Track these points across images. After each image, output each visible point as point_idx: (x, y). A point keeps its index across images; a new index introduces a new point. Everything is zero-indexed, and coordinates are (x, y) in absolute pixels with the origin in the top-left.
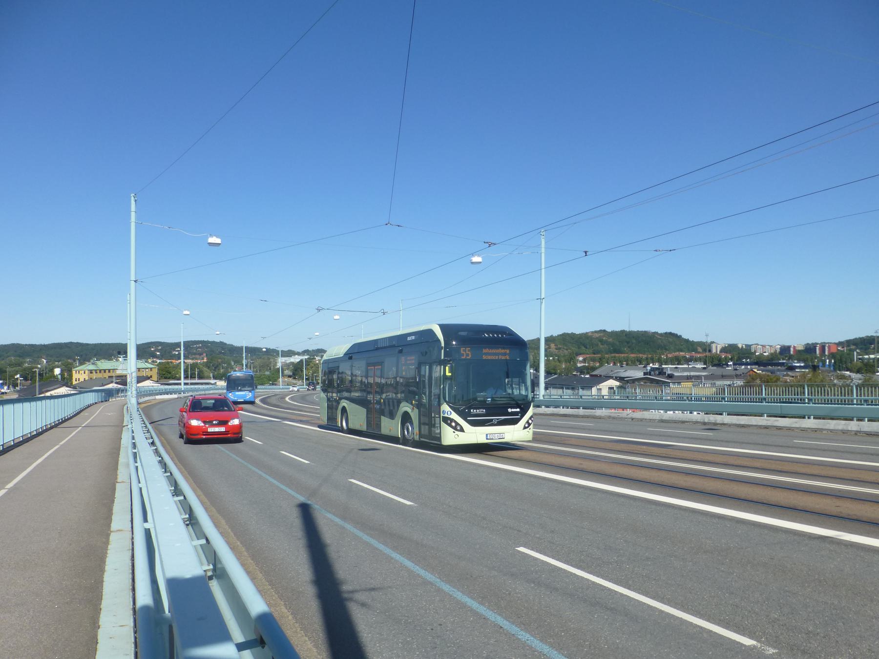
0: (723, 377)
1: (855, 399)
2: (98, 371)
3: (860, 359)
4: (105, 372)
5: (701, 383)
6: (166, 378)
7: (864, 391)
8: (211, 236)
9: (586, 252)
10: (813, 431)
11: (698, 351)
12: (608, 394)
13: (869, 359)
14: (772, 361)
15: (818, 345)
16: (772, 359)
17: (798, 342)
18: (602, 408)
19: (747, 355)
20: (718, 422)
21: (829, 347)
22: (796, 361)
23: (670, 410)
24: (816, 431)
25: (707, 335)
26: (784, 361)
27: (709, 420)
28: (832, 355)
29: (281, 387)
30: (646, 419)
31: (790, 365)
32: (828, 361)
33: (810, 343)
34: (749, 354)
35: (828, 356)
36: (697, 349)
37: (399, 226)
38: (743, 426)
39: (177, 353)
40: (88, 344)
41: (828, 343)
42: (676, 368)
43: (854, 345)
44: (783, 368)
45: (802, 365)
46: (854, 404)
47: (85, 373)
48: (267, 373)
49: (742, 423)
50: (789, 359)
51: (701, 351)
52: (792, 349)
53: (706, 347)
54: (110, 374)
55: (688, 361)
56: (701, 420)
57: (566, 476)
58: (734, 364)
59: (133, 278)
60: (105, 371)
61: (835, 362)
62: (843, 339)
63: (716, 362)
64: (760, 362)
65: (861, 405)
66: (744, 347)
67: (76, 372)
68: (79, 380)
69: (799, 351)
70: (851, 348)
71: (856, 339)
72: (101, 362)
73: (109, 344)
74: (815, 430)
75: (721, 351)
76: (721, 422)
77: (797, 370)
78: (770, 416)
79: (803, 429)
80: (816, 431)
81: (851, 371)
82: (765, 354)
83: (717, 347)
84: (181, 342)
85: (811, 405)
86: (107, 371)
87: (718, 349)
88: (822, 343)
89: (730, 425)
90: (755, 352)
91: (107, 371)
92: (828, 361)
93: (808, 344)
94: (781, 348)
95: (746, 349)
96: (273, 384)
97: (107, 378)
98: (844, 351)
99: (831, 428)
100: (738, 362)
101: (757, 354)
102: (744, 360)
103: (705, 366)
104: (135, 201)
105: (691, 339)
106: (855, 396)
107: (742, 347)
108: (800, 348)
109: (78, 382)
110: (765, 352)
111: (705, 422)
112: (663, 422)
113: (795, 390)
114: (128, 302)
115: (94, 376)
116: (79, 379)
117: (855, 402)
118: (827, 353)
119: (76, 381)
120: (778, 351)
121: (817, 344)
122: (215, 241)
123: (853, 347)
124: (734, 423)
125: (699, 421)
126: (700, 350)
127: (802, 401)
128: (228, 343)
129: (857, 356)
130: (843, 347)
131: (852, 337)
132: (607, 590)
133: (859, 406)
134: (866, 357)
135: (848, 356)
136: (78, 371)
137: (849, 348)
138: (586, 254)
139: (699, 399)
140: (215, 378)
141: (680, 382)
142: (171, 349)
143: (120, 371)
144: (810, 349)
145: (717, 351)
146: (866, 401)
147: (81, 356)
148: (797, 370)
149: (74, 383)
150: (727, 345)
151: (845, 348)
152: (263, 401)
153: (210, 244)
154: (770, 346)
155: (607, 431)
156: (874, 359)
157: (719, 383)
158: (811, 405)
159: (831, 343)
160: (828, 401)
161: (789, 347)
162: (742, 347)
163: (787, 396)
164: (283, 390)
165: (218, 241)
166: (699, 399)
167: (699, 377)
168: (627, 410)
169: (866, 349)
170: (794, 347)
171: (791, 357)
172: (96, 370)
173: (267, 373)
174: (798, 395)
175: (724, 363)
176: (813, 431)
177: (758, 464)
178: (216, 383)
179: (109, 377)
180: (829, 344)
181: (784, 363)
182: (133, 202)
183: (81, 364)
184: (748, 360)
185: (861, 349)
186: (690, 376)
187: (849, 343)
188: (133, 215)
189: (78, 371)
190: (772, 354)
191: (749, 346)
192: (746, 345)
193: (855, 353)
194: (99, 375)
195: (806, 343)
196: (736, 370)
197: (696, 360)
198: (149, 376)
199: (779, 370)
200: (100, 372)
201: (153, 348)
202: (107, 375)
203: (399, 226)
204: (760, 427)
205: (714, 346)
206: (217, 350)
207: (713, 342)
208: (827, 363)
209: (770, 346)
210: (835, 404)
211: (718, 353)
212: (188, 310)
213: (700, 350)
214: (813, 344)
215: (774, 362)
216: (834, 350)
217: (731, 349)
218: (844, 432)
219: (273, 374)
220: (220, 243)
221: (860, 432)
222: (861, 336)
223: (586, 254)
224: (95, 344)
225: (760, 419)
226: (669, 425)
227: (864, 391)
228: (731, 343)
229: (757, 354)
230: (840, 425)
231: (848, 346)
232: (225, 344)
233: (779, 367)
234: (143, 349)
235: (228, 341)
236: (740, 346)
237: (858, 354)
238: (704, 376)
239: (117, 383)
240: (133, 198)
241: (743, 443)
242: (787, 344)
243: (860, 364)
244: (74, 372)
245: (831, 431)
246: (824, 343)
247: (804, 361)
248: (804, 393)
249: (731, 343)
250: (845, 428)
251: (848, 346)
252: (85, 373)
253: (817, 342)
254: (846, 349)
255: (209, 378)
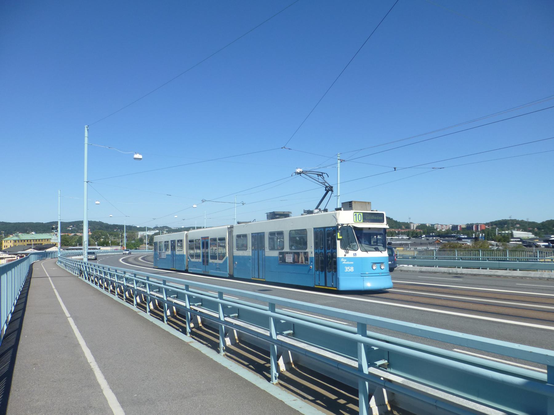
0: (421, 244)
1: (508, 258)
2: (20, 241)
3: (500, 233)
4: (24, 241)
5: (408, 248)
6: (65, 245)
7: (513, 253)
8: (136, 153)
9: (395, 168)
10: (520, 278)
11: (403, 228)
12: (262, 251)
13: (505, 233)
14: (448, 234)
15: (474, 225)
16: (447, 233)
17: (462, 223)
18: (552, 270)
19: (432, 231)
20: (458, 272)
21: (481, 226)
22: (462, 235)
23: (411, 265)
24: (522, 278)
25: (410, 218)
26: (455, 235)
27: (452, 271)
28: (483, 231)
29: (147, 251)
30: (410, 271)
31: (458, 237)
32: (481, 234)
33: (469, 223)
34: (433, 230)
35: (480, 231)
36: (402, 227)
37: (289, 149)
38: (475, 275)
39: (70, 229)
40: (10, 223)
41: (480, 224)
42: (392, 238)
43: (495, 225)
44: (455, 239)
45: (466, 237)
46: (434, 259)
47: (11, 242)
48: (133, 242)
49: (474, 273)
50: (457, 233)
51: (404, 228)
52: (459, 227)
53: (407, 225)
54: (29, 243)
55: (398, 234)
56: (447, 271)
57: (415, 306)
58: (426, 236)
59: (86, 180)
60: (24, 241)
61: (485, 236)
62: (488, 221)
63: (415, 235)
64: (441, 235)
65: (486, 261)
66: (430, 226)
67: (5, 241)
68: (7, 247)
69: (463, 228)
70: (494, 227)
71: (496, 221)
72: (22, 235)
73: (25, 223)
74: (522, 278)
75: (416, 228)
76: (460, 273)
77: (463, 240)
78: (418, 266)
79: (514, 277)
80: (522, 278)
81: (495, 241)
82: (443, 230)
83: (414, 226)
84: (82, 222)
85: (437, 260)
86: (26, 241)
87: (415, 226)
88: (476, 224)
89: (466, 274)
90: (437, 229)
91: (26, 241)
92: (481, 234)
93: (468, 224)
94: (452, 227)
95: (431, 227)
96: (136, 249)
97: (26, 245)
98: (489, 228)
99: (532, 276)
100: (428, 235)
101: (438, 230)
102: (431, 234)
103: (408, 238)
104: (88, 130)
105: (398, 221)
106: (481, 256)
107: (429, 226)
108: (464, 226)
109: (6, 248)
110: (443, 229)
111: (450, 273)
112: (421, 272)
113: (474, 252)
114: (59, 195)
115: (17, 244)
116: (7, 246)
117: (481, 259)
118: (479, 230)
119: (5, 247)
120: (451, 228)
121: (474, 224)
122: (138, 157)
123: (494, 226)
124: (469, 273)
125: (446, 272)
126: (403, 227)
127: (479, 259)
128: (104, 222)
129: (498, 232)
130: (489, 226)
131: (494, 220)
132: (248, 382)
133: (458, 261)
134: (503, 232)
135: (492, 232)
136: (6, 241)
137: (492, 227)
138: (395, 169)
139: (406, 258)
140: (98, 245)
141: (396, 247)
142: (66, 226)
143: (53, 240)
144: (469, 227)
145: (414, 228)
146: (488, 259)
147: (5, 231)
148: (463, 240)
149: (3, 248)
150: (420, 225)
151: (490, 227)
152: (143, 259)
153: (135, 159)
154: (441, 225)
155: (395, 278)
156: (507, 234)
157: (419, 248)
158: (437, 260)
159: (481, 224)
160: (471, 259)
161: (457, 226)
162: (429, 226)
163: (470, 257)
164: (148, 253)
165: (140, 157)
166: (406, 258)
167: (407, 244)
168: (552, 272)
169: (502, 228)
170: (460, 226)
171: (458, 232)
172: (18, 240)
173: (133, 242)
174: (476, 256)
175: (419, 235)
176: (520, 278)
177: (516, 298)
178: (100, 248)
179: (27, 245)
180: (481, 225)
181: (455, 236)
182: (86, 131)
183: (6, 236)
184: (433, 234)
185: (499, 227)
186: (402, 243)
187: (492, 224)
188: (86, 139)
189: (6, 241)
190: (447, 230)
191: (433, 225)
192: (431, 225)
193: (497, 230)
194: (21, 244)
195: (467, 224)
196: (428, 240)
197: (403, 234)
198: (54, 244)
199: (452, 240)
200: (21, 241)
201: (54, 225)
202: (26, 243)
203: (289, 149)
204: (486, 275)
205: (412, 225)
206: (98, 227)
207: (412, 223)
208: (480, 236)
209: (441, 225)
210: (472, 260)
211: (415, 229)
212: (99, 201)
213: (403, 227)
214: (471, 224)
215: (449, 235)
216: (483, 228)
217: (422, 227)
218: (540, 279)
219: (137, 242)
220: (142, 158)
221: (550, 278)
222: (499, 220)
223: (395, 169)
224: (15, 223)
225: (486, 271)
226: (431, 274)
227: (513, 253)
228: (422, 223)
229: (438, 230)
230: (475, 271)
231: (492, 225)
232: (103, 223)
233: (453, 238)
234: (48, 226)
235: (105, 221)
236: (428, 225)
237: (498, 231)
238: (409, 243)
239: (34, 249)
240: (86, 128)
241: (489, 285)
242: (456, 224)
243: (500, 237)
244: (3, 241)
245: (532, 278)
246: (478, 223)
247: (467, 235)
248: (479, 254)
249: (422, 223)
250: (541, 276)
251: (492, 225)
252: (11, 242)
253: (473, 223)
254: (491, 228)
255: (95, 245)
